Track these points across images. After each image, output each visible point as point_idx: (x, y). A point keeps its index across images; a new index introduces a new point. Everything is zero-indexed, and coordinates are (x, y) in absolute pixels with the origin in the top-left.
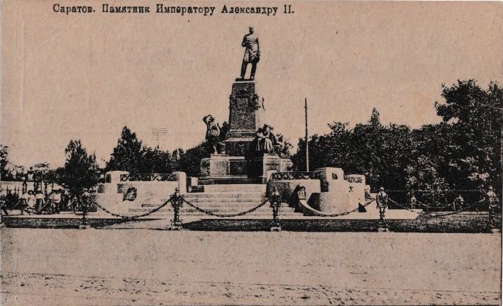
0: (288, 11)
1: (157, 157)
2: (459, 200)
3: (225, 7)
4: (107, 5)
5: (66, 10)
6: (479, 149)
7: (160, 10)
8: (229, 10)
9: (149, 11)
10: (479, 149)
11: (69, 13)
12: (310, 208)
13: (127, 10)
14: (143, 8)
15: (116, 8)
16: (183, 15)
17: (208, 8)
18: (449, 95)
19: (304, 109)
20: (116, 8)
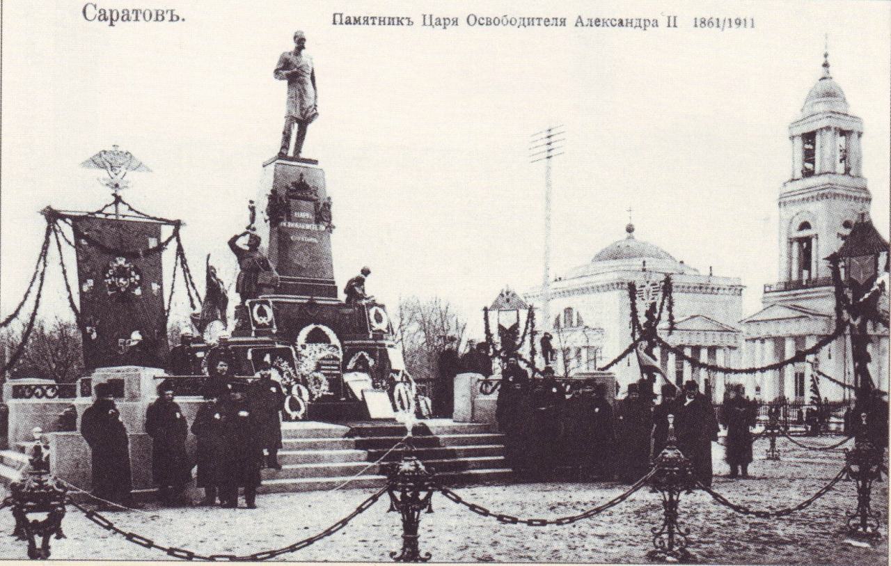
0: (672, 24)
1: (876, 306)
2: (678, 540)
3: (580, 17)
4: (341, 15)
5: (442, 22)
6: (195, 470)
7: (530, 20)
8: (585, 22)
9: (564, 25)
10: (195, 470)
11: (447, 27)
12: (363, 439)
13: (370, 21)
14: (389, 24)
15: (355, 18)
16: (445, 28)
17: (448, 19)
18: (220, 339)
19: (175, 285)
20: (355, 18)
